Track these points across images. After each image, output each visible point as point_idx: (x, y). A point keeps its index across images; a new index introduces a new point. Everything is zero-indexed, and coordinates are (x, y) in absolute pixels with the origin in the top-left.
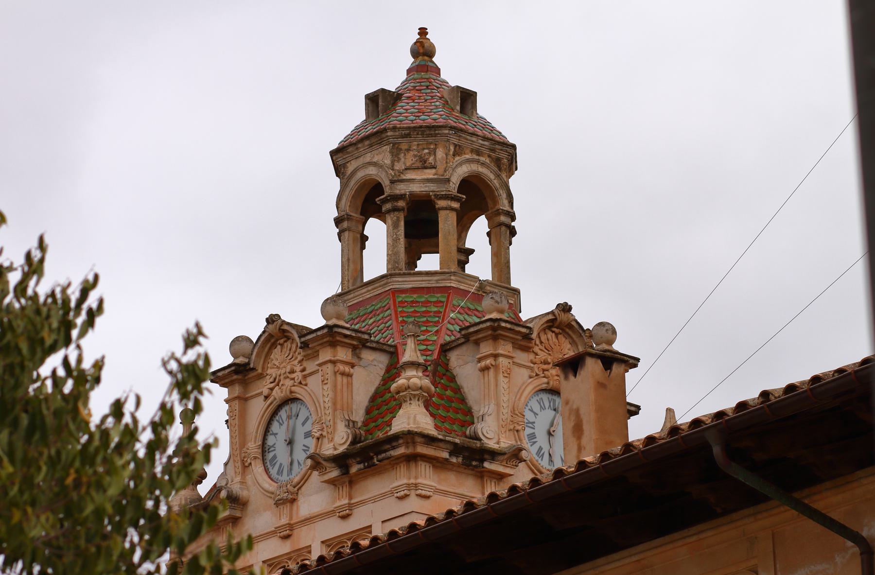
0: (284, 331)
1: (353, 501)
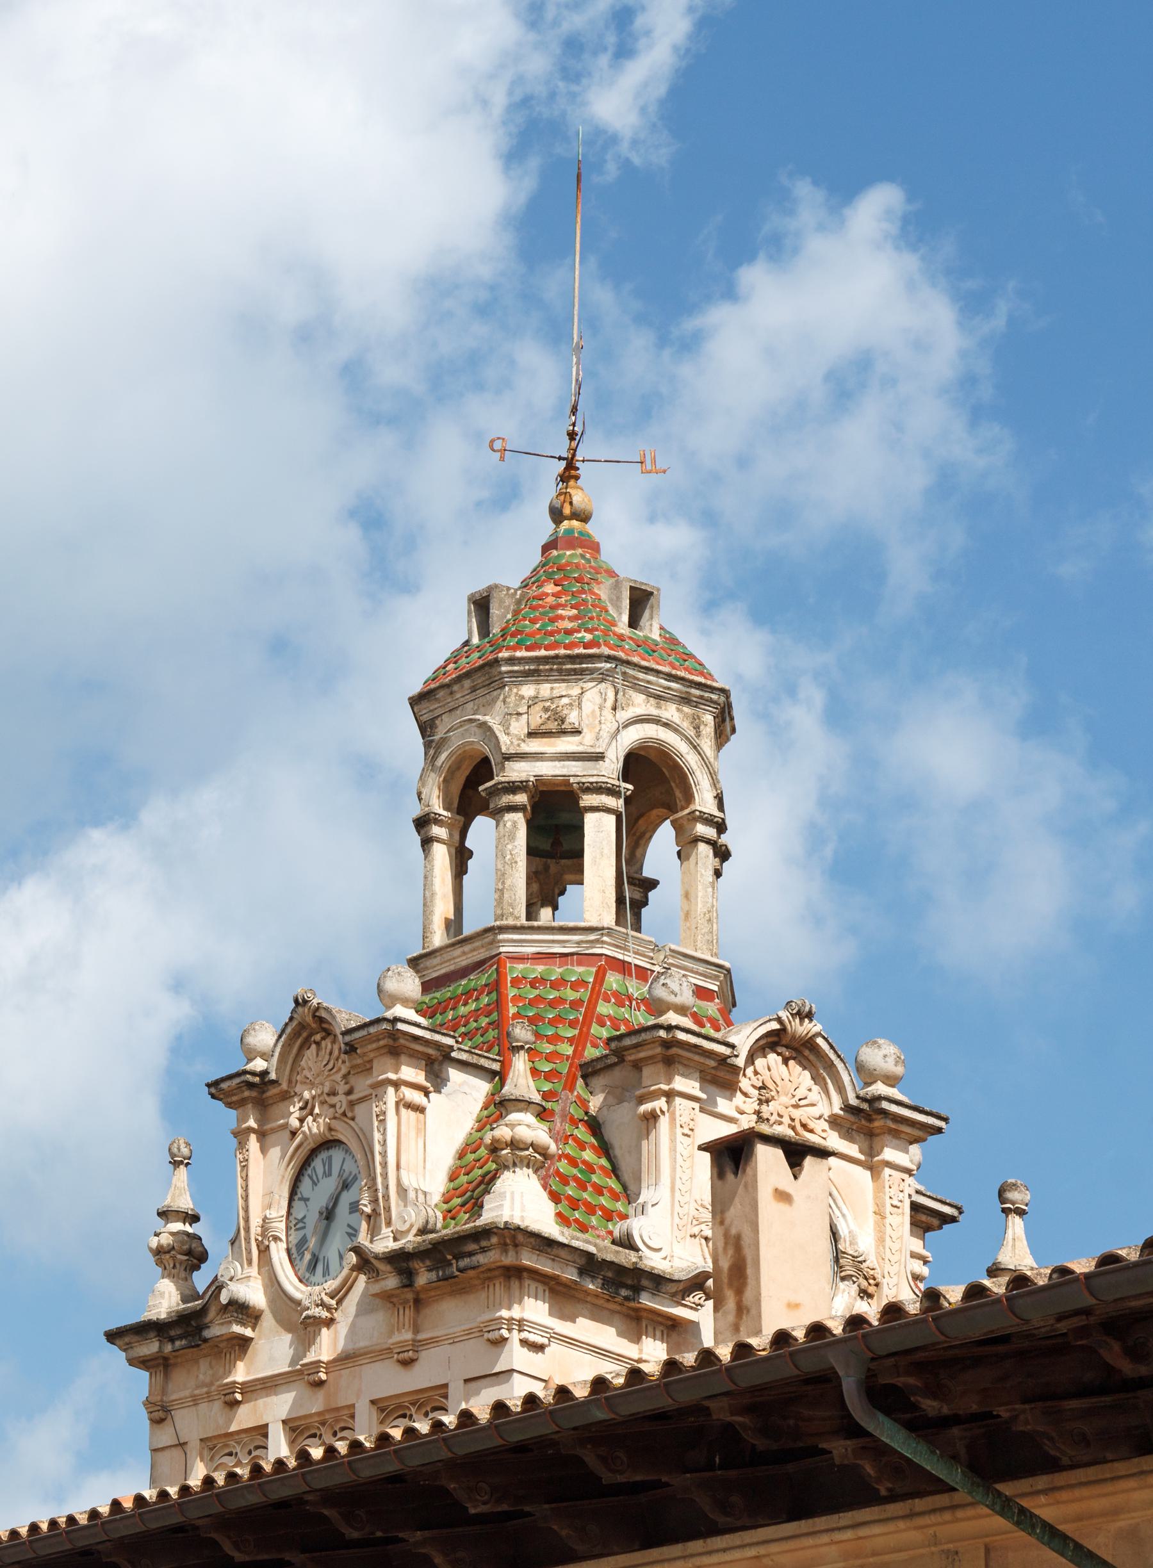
0: (321, 1020)
1: (420, 1337)
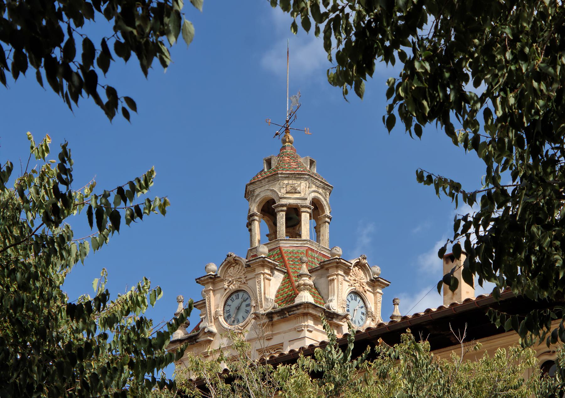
0: (235, 260)
